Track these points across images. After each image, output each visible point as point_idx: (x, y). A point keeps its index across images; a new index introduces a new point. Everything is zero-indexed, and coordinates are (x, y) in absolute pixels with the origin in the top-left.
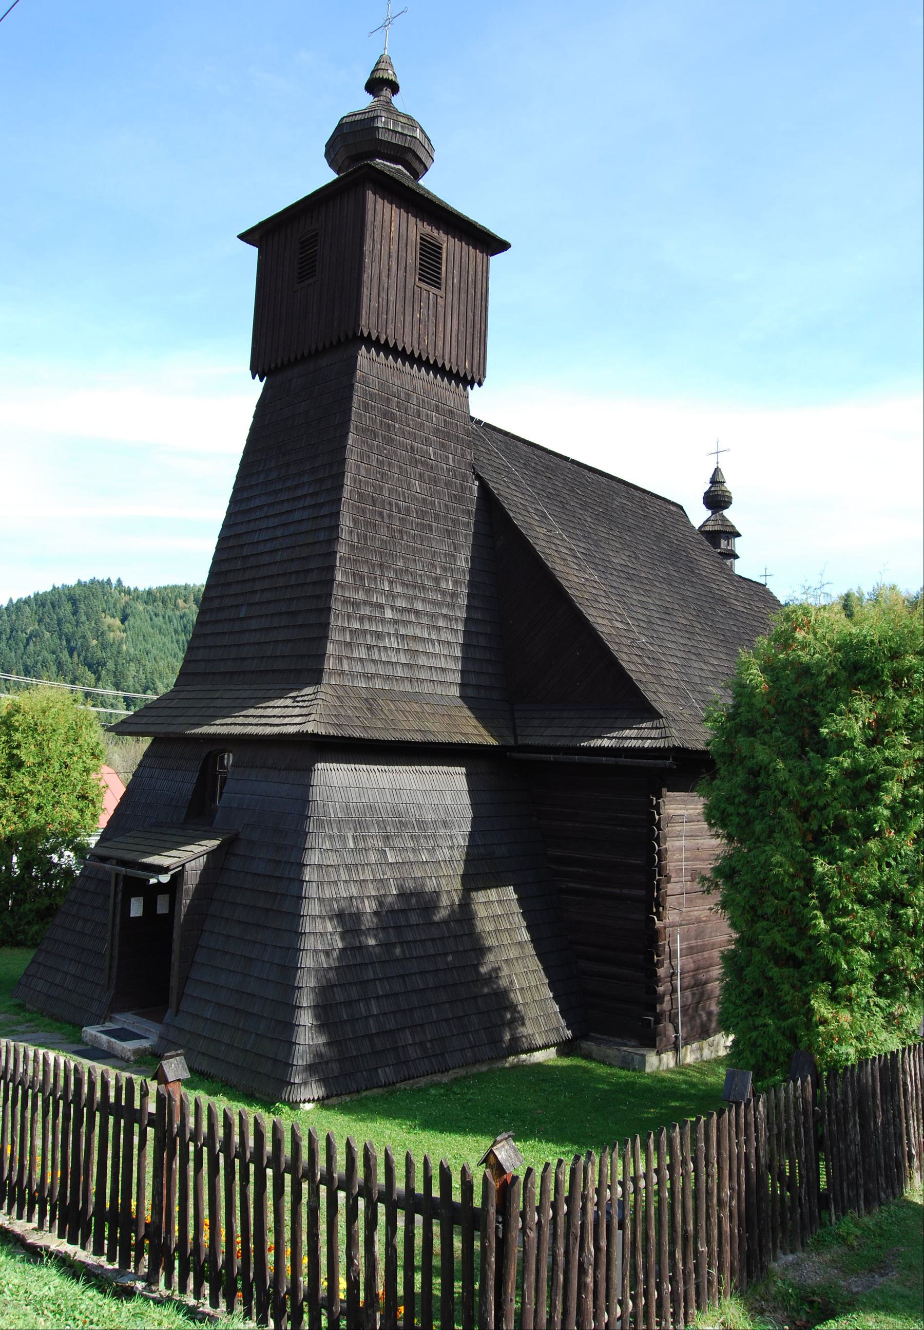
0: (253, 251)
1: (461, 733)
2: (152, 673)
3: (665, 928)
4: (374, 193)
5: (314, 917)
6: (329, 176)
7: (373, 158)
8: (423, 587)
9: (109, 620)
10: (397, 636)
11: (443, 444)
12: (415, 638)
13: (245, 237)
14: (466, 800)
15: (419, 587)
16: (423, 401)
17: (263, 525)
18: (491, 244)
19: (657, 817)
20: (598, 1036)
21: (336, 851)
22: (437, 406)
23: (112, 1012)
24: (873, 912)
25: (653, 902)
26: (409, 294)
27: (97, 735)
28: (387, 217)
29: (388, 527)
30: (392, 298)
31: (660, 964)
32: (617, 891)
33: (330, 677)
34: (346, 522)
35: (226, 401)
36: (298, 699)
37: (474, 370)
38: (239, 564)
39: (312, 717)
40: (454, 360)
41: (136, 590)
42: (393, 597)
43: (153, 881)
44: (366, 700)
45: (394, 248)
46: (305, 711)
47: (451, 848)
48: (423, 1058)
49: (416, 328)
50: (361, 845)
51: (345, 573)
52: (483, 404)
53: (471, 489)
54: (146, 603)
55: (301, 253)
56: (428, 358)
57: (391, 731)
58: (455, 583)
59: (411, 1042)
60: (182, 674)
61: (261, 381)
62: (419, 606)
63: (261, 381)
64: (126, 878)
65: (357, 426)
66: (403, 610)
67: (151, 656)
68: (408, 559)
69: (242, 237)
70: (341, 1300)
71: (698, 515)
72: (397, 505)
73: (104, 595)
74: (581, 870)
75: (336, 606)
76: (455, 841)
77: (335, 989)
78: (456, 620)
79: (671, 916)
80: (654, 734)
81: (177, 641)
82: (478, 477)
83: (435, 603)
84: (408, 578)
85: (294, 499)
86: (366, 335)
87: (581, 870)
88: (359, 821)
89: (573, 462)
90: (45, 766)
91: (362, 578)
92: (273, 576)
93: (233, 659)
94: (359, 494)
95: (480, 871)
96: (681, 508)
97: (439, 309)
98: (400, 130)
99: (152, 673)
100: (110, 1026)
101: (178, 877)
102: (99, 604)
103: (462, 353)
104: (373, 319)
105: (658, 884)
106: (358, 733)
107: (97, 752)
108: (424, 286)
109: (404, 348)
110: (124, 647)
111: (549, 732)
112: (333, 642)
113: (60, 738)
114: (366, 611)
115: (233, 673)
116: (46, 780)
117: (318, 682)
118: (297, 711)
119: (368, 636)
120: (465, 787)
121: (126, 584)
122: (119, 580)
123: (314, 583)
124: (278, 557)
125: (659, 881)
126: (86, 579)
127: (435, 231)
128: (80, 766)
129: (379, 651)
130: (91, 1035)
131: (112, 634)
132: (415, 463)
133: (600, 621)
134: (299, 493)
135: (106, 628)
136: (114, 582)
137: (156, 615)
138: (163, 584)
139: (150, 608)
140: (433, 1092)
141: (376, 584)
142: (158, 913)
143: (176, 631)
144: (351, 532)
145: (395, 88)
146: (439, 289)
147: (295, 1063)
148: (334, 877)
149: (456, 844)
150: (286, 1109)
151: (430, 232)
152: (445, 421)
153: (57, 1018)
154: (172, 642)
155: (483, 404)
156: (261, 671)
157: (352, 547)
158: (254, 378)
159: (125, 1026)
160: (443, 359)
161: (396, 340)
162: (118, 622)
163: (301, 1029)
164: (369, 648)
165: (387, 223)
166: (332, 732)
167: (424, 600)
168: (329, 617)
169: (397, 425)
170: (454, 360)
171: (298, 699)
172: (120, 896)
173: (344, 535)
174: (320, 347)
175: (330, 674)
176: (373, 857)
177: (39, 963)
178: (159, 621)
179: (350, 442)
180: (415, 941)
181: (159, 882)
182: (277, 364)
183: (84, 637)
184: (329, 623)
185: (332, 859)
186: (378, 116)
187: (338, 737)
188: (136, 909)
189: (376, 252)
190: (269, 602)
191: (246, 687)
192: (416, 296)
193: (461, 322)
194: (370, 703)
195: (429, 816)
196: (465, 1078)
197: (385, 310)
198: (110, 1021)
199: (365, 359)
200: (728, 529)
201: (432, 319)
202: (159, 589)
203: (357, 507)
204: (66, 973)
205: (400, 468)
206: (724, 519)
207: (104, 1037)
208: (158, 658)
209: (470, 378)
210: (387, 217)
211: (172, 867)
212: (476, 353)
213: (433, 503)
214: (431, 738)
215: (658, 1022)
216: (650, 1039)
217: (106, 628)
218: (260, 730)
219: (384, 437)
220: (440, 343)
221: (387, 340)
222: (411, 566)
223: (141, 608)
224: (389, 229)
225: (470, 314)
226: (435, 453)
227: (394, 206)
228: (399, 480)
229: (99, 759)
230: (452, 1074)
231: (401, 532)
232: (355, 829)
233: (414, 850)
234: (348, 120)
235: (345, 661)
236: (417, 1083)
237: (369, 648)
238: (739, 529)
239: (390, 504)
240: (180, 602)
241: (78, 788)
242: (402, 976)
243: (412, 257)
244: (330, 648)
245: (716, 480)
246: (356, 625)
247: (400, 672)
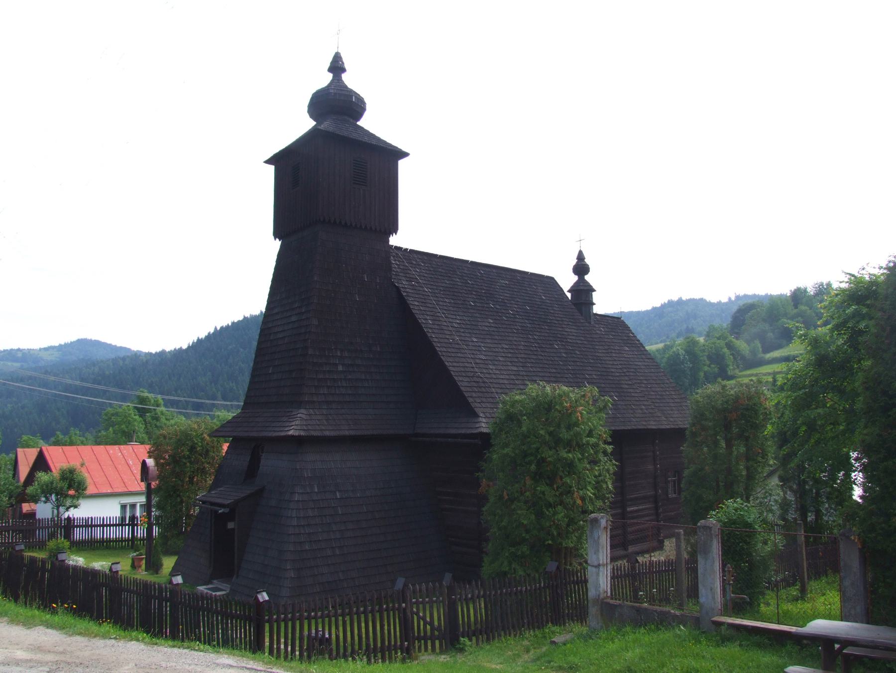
0: (272, 168)
6: (310, 124)
13: (268, 162)
100: (210, 586)
145: (344, 70)
237: (328, 387)
238: (594, 287)
245: (581, 257)
246: (321, 376)
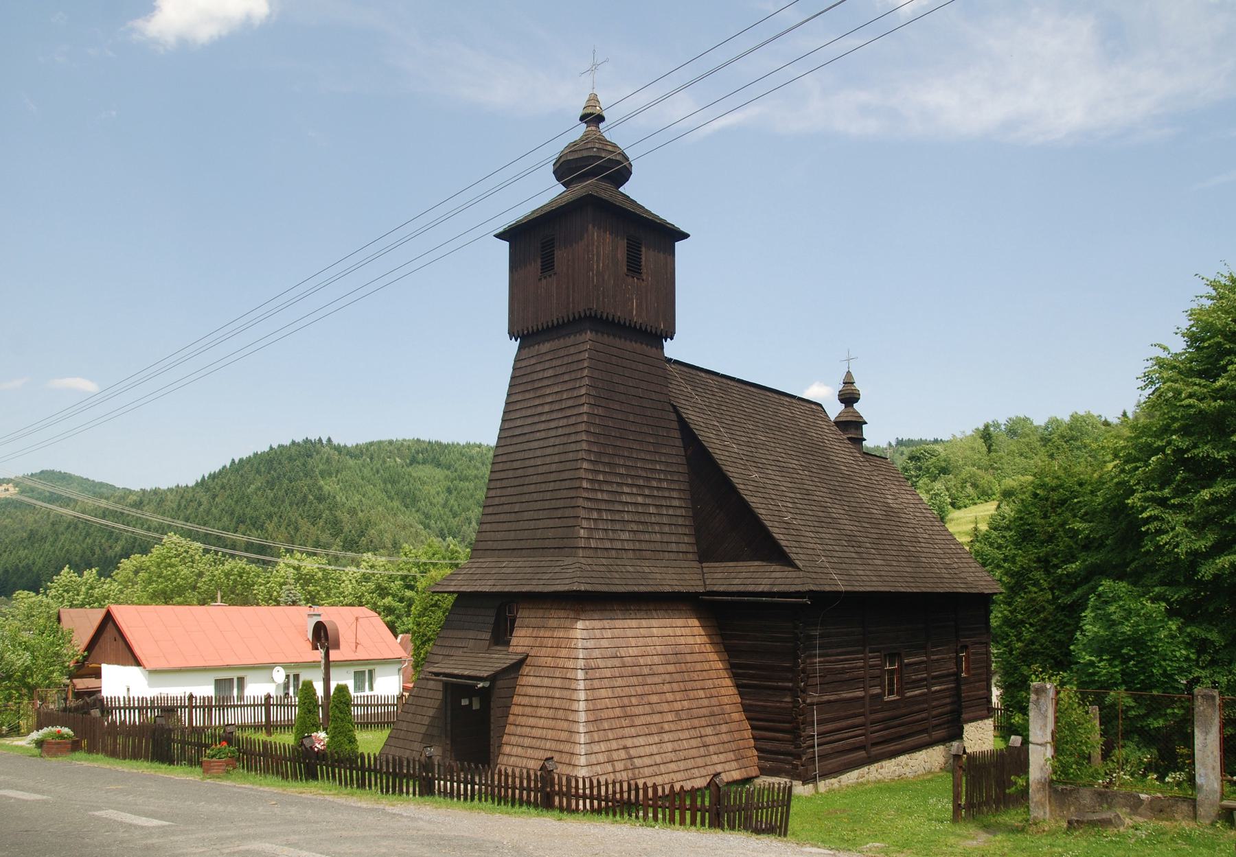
18: (670, 235)
24: (1117, 752)
52: (671, 349)
64: (453, 684)
71: (834, 409)
89: (739, 381)
96: (820, 405)
121: (335, 442)
122: (329, 440)
155: (671, 349)
166: (589, 588)
238: (866, 419)
245: (849, 382)
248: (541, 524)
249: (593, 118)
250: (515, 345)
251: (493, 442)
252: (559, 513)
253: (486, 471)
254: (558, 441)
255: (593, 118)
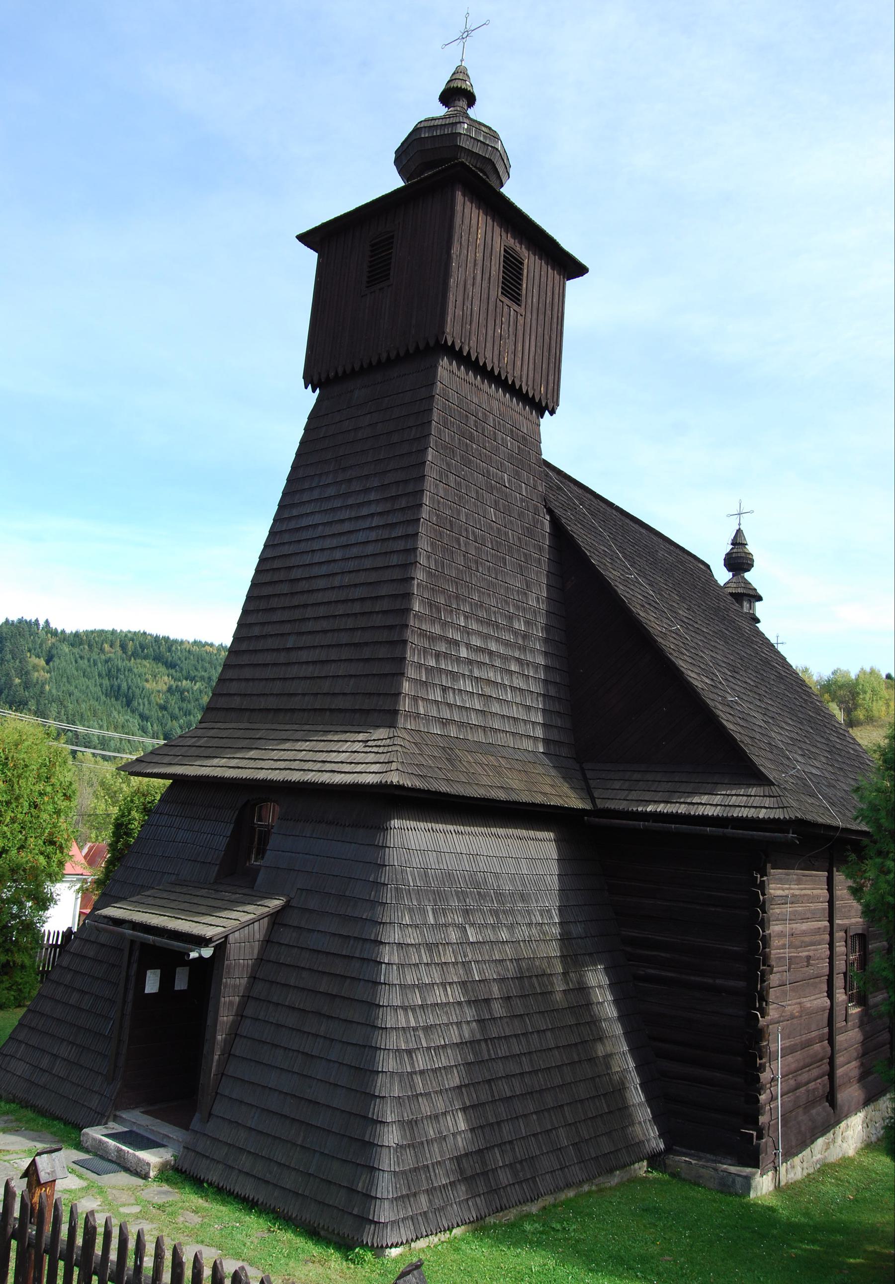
1: (541, 793)
2: (74, 715)
3: (768, 1026)
4: (464, 195)
5: (395, 1008)
6: (394, 182)
7: (450, 164)
8: (497, 626)
9: (34, 660)
10: (471, 677)
11: (517, 471)
12: (488, 681)
13: (306, 238)
14: (554, 868)
15: (493, 625)
16: (499, 423)
17: (316, 545)
19: (761, 898)
20: (684, 1150)
21: (417, 926)
22: (512, 431)
23: (116, 1110)
25: (754, 997)
26: (491, 307)
27: (70, 774)
28: (474, 222)
29: (464, 556)
30: (476, 309)
31: (762, 1068)
32: (710, 981)
33: (405, 720)
34: (423, 544)
35: (271, 413)
36: (370, 743)
37: (549, 396)
38: (285, 588)
39: (394, 766)
40: (530, 383)
41: (63, 632)
42: (468, 633)
43: (193, 955)
44: (443, 748)
45: (479, 255)
46: (382, 758)
47: (530, 925)
48: (513, 1184)
49: (497, 343)
50: (442, 920)
51: (422, 602)
53: (542, 523)
54: (72, 645)
55: (372, 257)
56: (506, 377)
57: (475, 787)
58: (528, 623)
59: (501, 1164)
60: (209, 710)
61: (314, 391)
62: (493, 646)
63: (314, 391)
64: (144, 946)
65: (436, 441)
66: (479, 650)
67: (73, 698)
68: (483, 593)
69: (303, 238)
70: (15, 1218)
71: (722, 576)
72: (473, 532)
73: (30, 635)
74: (663, 955)
75: (413, 639)
76: (533, 917)
77: (420, 1099)
78: (528, 665)
79: (773, 1013)
80: (767, 802)
81: (101, 685)
82: (550, 511)
83: (507, 644)
84: (482, 614)
85: (357, 518)
86: (449, 344)
87: (663, 955)
88: (439, 890)
90: (14, 805)
91: (439, 610)
92: (329, 603)
93: (277, 695)
94: (438, 516)
95: (574, 954)
96: (708, 567)
97: (519, 327)
98: (482, 139)
99: (74, 715)
101: (221, 948)
102: (24, 644)
103: (538, 377)
104: (458, 328)
105: (763, 975)
106: (444, 788)
107: (69, 792)
108: (506, 301)
109: (485, 363)
110: (47, 688)
111: (634, 795)
112: (410, 679)
113: (32, 776)
114: (442, 647)
115: (278, 710)
116: (13, 820)
117: (392, 725)
118: (371, 758)
119: (444, 676)
120: (555, 856)
121: (53, 625)
122: (47, 622)
123: (384, 612)
124: (337, 581)
125: (763, 972)
126: (14, 617)
127: (518, 245)
128: (50, 808)
129: (454, 693)
130: (94, 1139)
131: (36, 674)
132: (490, 489)
133: (690, 673)
134: (365, 511)
135: (30, 668)
136: (42, 623)
137: (81, 658)
138: (90, 627)
139: (76, 650)
140: (528, 1227)
141: (452, 618)
142: (176, 989)
143: (100, 675)
144: (429, 558)
145: (471, 99)
146: (519, 305)
147: (379, 1196)
148: (415, 959)
149: (534, 921)
150: (369, 1256)
151: (512, 245)
152: (519, 447)
153: (42, 1112)
154: (96, 685)
156: (315, 710)
157: (430, 574)
158: (306, 388)
159: (135, 1129)
160: (521, 381)
161: (478, 353)
162: (42, 662)
163: (385, 1151)
164: (444, 689)
165: (474, 229)
166: (418, 784)
167: (498, 640)
168: (405, 652)
169: (474, 446)
170: (530, 383)
171: (370, 743)
172: (135, 967)
173: (422, 560)
174: (393, 355)
175: (406, 716)
176: (453, 936)
177: (21, 1042)
178: (83, 664)
179: (430, 458)
180: (499, 1038)
181: (201, 957)
182: (337, 373)
183: (8, 675)
184: (405, 658)
185: (412, 937)
186: (460, 122)
187: (424, 790)
188: (152, 984)
189: (463, 257)
190: (325, 632)
191: (296, 727)
192: (498, 310)
193: (538, 344)
194: (449, 751)
195: (508, 887)
196: (554, 1206)
197: (469, 320)
198: (114, 1121)
199: (446, 371)
200: (751, 593)
201: (512, 337)
202: (88, 633)
203: (435, 530)
204: (56, 1056)
205: (477, 492)
206: (747, 583)
207: (112, 1143)
208: (80, 700)
209: (544, 405)
210: (474, 222)
211: (215, 939)
212: (551, 378)
213: (506, 534)
214: (514, 797)
215: (760, 1137)
216: (751, 1158)
217: (30, 668)
218: (326, 778)
219: (462, 457)
220: (519, 363)
221: (469, 353)
222: (486, 600)
223: (67, 650)
224: (475, 238)
225: (547, 337)
226: (509, 481)
227: (481, 212)
228: (475, 505)
229: (70, 801)
230: (540, 1203)
231: (477, 562)
232: (435, 900)
233: (493, 927)
234: (426, 124)
235: (420, 703)
236: (506, 1216)
237: (444, 689)
238: (760, 592)
239: (466, 530)
240: (106, 647)
241: (47, 831)
242: (489, 1082)
243: (496, 268)
244: (406, 687)
245: (738, 541)
246: (432, 663)
247: (474, 720)
248: (331, 669)
249: (457, 94)
250: (310, 398)
251: (227, 640)
252: (367, 653)
253: (215, 674)
254: (373, 536)
255: (457, 94)
